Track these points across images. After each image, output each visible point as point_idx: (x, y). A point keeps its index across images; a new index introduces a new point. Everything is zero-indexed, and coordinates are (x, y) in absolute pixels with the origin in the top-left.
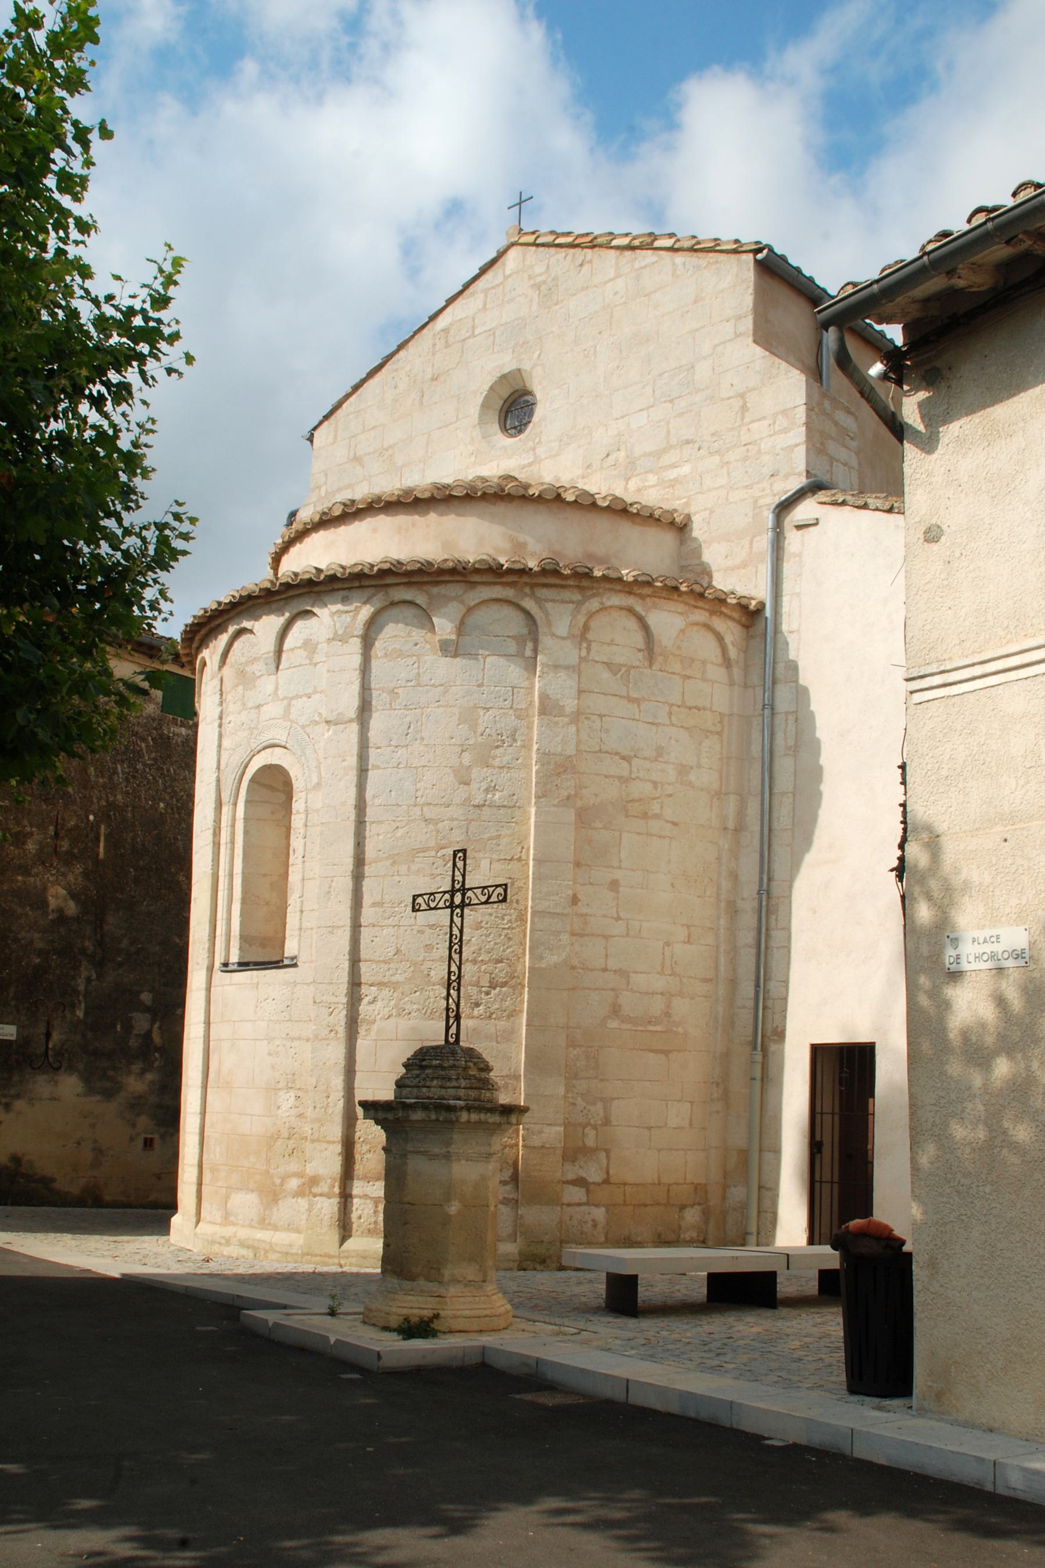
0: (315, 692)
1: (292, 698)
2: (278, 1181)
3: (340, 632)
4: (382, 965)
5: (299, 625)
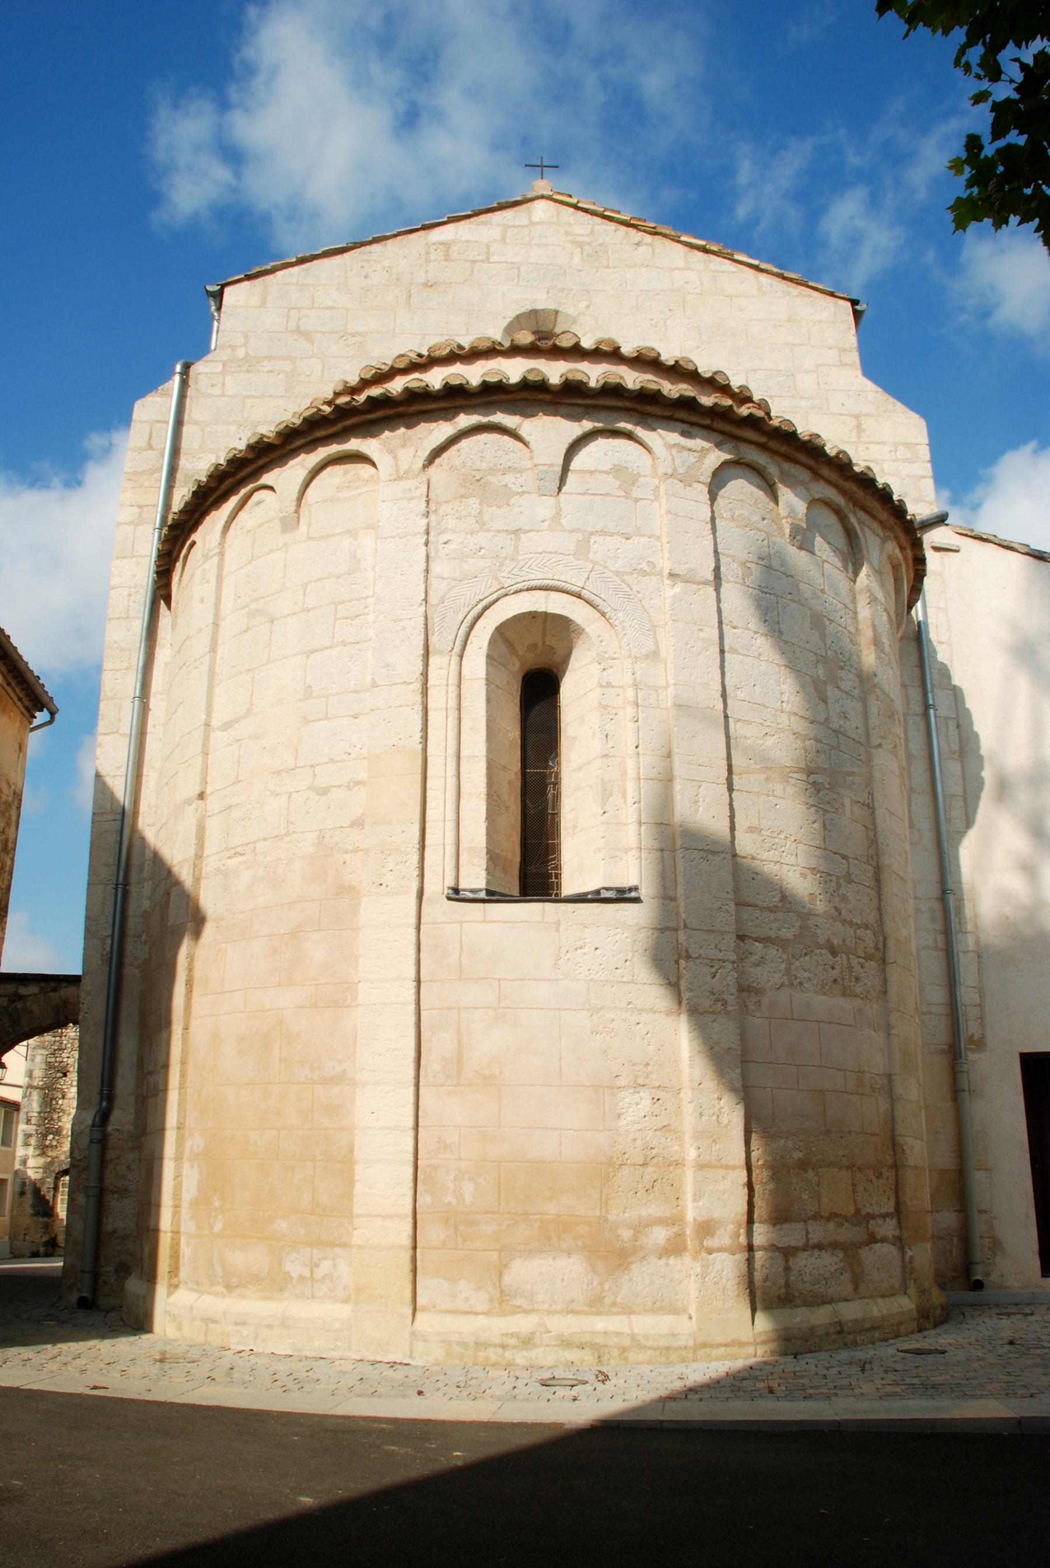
0: (639, 533)
1: (592, 534)
2: (627, 1234)
3: (681, 470)
4: (767, 914)
5: (601, 444)
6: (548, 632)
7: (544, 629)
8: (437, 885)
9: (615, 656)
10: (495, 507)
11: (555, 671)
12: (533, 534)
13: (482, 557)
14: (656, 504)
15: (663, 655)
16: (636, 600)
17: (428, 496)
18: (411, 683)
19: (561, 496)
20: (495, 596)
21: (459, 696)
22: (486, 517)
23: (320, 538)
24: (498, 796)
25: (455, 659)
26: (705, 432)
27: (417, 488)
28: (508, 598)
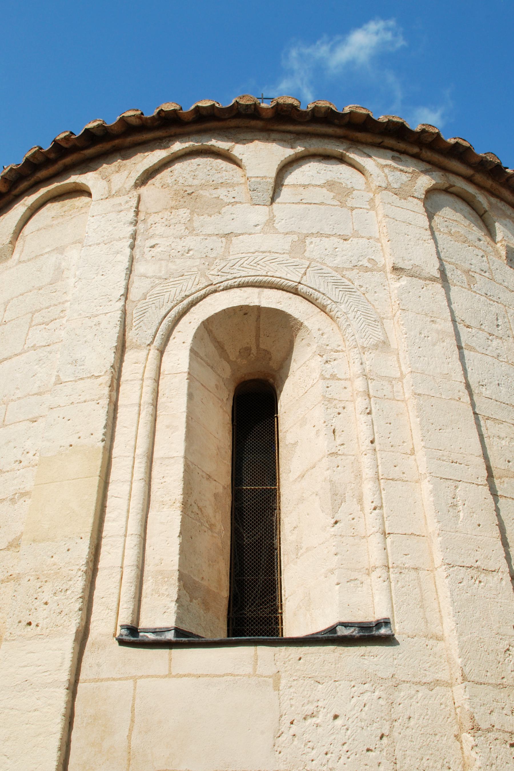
0: (356, 235)
1: (307, 236)
6: (261, 333)
7: (258, 329)
8: (106, 625)
9: (339, 348)
10: (206, 216)
11: (271, 380)
12: (245, 237)
16: (358, 293)
17: (137, 207)
19: (274, 205)
20: (203, 292)
21: (156, 392)
22: (196, 224)
23: (29, 260)
25: (154, 353)
26: (415, 161)
27: (127, 202)
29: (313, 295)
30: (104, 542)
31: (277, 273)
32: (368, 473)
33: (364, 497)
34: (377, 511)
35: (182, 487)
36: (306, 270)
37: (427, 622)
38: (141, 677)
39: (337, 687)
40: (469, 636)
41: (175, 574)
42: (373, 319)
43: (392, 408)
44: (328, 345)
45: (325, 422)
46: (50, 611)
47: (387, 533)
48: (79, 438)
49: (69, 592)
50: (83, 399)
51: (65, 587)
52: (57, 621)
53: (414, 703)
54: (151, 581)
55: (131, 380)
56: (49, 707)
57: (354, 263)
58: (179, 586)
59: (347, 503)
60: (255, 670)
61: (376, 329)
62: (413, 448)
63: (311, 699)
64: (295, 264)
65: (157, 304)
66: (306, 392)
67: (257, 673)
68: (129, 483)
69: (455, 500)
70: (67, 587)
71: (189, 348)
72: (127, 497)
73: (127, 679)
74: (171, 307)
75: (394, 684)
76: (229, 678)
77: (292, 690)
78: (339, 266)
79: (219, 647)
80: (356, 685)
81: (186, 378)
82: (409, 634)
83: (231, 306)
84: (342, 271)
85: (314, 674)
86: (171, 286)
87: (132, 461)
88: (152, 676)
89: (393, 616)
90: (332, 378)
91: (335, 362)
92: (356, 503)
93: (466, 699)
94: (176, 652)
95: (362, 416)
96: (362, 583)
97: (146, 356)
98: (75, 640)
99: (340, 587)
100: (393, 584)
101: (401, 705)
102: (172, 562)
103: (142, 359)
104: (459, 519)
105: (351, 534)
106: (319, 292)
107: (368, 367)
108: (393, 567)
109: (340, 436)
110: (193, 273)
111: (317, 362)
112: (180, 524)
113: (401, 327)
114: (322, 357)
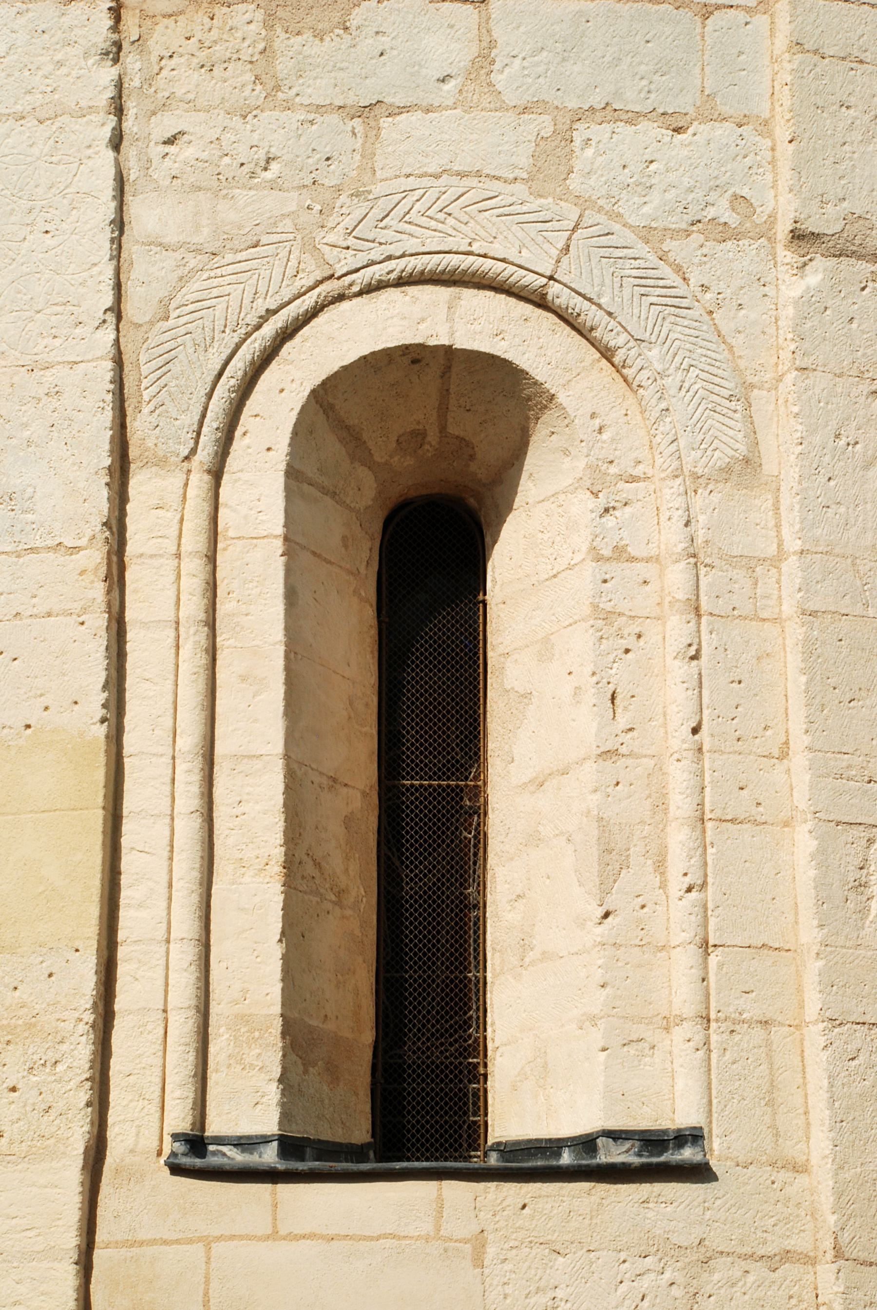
7: (445, 394)
8: (141, 1129)
9: (639, 471)
10: (307, 35)
11: (472, 502)
13: (273, 186)
14: (761, 21)
15: (769, 467)
18: (76, 549)
21: (212, 586)
22: (283, 66)
24: (317, 865)
25: (199, 482)
28: (345, 305)
29: (582, 317)
30: (122, 952)
31: (496, 245)
32: (680, 804)
33: (669, 857)
34: (694, 894)
35: (282, 829)
36: (569, 239)
37: (777, 1135)
38: (219, 1239)
39: (592, 1263)
40: (859, 1170)
41: (275, 1022)
42: (726, 393)
43: (748, 642)
44: (611, 462)
45: (594, 674)
46: (24, 1106)
47: (711, 943)
48: (46, 708)
49: (60, 1068)
50: (42, 609)
51: (51, 1056)
52: (43, 1127)
53: (738, 1294)
54: (226, 1036)
55: (152, 556)
56: (42, 1298)
57: (694, 213)
58: (284, 1048)
59: (632, 871)
60: (438, 1229)
61: (731, 423)
62: (787, 743)
63: (542, 1284)
64: (541, 216)
65: (198, 336)
66: (555, 576)
67: (441, 1233)
68: (168, 820)
69: (865, 871)
70: (57, 1057)
71: (283, 466)
72: (166, 854)
73: (190, 1241)
74: (233, 346)
75: (701, 1257)
76: (389, 1243)
77: (508, 1266)
78: (654, 225)
79: (370, 1182)
80: (629, 1259)
81: (280, 552)
82: (739, 1159)
83: (378, 348)
84: (662, 241)
85: (549, 1237)
86: (228, 279)
87: (171, 766)
88: (241, 1237)
89: (711, 1122)
90: (615, 556)
91: (627, 509)
92: (651, 869)
93: (837, 1293)
94: (285, 1190)
95: (677, 663)
96: (653, 1047)
97: (181, 491)
98: (83, 1168)
99: (608, 1056)
100: (714, 1056)
101: (712, 1298)
102: (269, 997)
103: (174, 499)
104: (867, 917)
105: (637, 942)
106: (599, 306)
107: (701, 532)
108: (717, 1020)
109: (625, 708)
110: (284, 237)
111: (583, 506)
112: (281, 913)
113: (792, 421)
114: (597, 497)
